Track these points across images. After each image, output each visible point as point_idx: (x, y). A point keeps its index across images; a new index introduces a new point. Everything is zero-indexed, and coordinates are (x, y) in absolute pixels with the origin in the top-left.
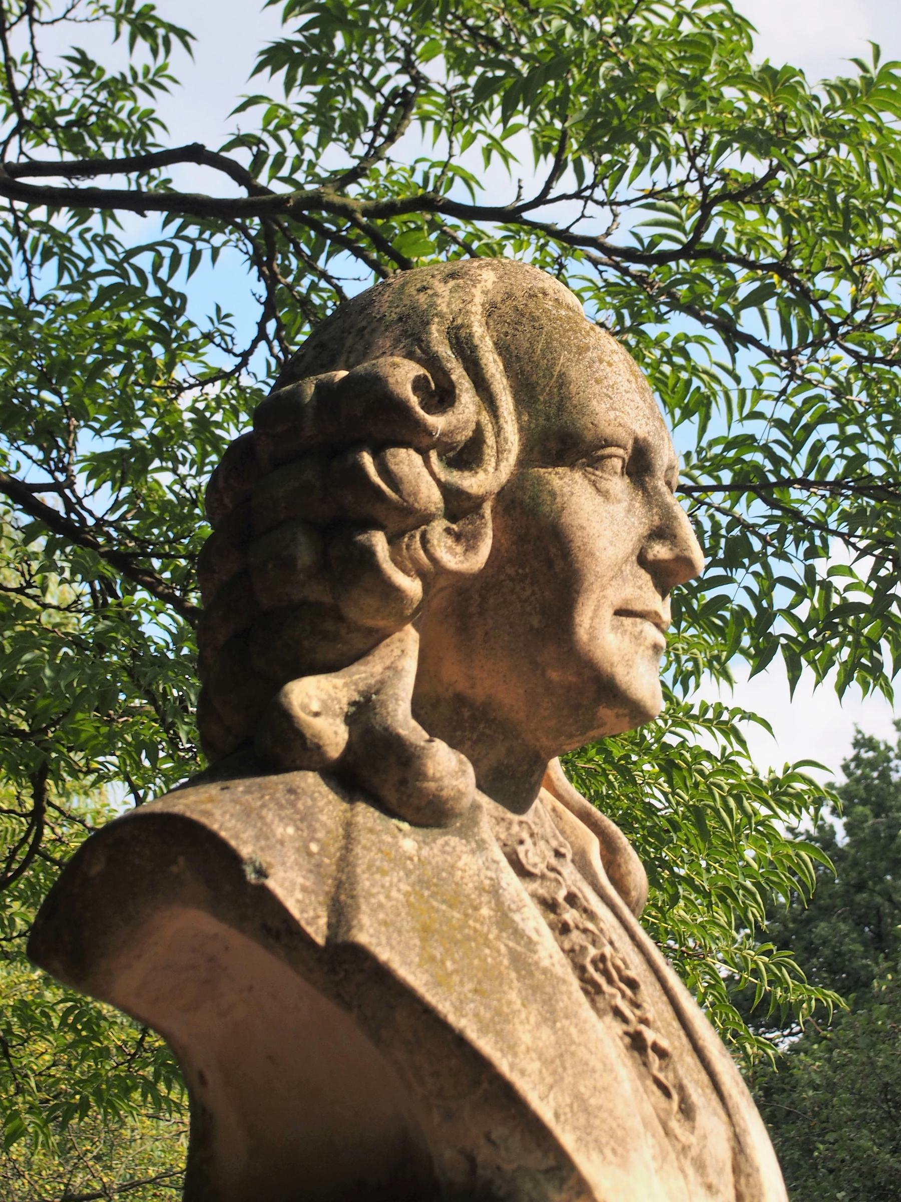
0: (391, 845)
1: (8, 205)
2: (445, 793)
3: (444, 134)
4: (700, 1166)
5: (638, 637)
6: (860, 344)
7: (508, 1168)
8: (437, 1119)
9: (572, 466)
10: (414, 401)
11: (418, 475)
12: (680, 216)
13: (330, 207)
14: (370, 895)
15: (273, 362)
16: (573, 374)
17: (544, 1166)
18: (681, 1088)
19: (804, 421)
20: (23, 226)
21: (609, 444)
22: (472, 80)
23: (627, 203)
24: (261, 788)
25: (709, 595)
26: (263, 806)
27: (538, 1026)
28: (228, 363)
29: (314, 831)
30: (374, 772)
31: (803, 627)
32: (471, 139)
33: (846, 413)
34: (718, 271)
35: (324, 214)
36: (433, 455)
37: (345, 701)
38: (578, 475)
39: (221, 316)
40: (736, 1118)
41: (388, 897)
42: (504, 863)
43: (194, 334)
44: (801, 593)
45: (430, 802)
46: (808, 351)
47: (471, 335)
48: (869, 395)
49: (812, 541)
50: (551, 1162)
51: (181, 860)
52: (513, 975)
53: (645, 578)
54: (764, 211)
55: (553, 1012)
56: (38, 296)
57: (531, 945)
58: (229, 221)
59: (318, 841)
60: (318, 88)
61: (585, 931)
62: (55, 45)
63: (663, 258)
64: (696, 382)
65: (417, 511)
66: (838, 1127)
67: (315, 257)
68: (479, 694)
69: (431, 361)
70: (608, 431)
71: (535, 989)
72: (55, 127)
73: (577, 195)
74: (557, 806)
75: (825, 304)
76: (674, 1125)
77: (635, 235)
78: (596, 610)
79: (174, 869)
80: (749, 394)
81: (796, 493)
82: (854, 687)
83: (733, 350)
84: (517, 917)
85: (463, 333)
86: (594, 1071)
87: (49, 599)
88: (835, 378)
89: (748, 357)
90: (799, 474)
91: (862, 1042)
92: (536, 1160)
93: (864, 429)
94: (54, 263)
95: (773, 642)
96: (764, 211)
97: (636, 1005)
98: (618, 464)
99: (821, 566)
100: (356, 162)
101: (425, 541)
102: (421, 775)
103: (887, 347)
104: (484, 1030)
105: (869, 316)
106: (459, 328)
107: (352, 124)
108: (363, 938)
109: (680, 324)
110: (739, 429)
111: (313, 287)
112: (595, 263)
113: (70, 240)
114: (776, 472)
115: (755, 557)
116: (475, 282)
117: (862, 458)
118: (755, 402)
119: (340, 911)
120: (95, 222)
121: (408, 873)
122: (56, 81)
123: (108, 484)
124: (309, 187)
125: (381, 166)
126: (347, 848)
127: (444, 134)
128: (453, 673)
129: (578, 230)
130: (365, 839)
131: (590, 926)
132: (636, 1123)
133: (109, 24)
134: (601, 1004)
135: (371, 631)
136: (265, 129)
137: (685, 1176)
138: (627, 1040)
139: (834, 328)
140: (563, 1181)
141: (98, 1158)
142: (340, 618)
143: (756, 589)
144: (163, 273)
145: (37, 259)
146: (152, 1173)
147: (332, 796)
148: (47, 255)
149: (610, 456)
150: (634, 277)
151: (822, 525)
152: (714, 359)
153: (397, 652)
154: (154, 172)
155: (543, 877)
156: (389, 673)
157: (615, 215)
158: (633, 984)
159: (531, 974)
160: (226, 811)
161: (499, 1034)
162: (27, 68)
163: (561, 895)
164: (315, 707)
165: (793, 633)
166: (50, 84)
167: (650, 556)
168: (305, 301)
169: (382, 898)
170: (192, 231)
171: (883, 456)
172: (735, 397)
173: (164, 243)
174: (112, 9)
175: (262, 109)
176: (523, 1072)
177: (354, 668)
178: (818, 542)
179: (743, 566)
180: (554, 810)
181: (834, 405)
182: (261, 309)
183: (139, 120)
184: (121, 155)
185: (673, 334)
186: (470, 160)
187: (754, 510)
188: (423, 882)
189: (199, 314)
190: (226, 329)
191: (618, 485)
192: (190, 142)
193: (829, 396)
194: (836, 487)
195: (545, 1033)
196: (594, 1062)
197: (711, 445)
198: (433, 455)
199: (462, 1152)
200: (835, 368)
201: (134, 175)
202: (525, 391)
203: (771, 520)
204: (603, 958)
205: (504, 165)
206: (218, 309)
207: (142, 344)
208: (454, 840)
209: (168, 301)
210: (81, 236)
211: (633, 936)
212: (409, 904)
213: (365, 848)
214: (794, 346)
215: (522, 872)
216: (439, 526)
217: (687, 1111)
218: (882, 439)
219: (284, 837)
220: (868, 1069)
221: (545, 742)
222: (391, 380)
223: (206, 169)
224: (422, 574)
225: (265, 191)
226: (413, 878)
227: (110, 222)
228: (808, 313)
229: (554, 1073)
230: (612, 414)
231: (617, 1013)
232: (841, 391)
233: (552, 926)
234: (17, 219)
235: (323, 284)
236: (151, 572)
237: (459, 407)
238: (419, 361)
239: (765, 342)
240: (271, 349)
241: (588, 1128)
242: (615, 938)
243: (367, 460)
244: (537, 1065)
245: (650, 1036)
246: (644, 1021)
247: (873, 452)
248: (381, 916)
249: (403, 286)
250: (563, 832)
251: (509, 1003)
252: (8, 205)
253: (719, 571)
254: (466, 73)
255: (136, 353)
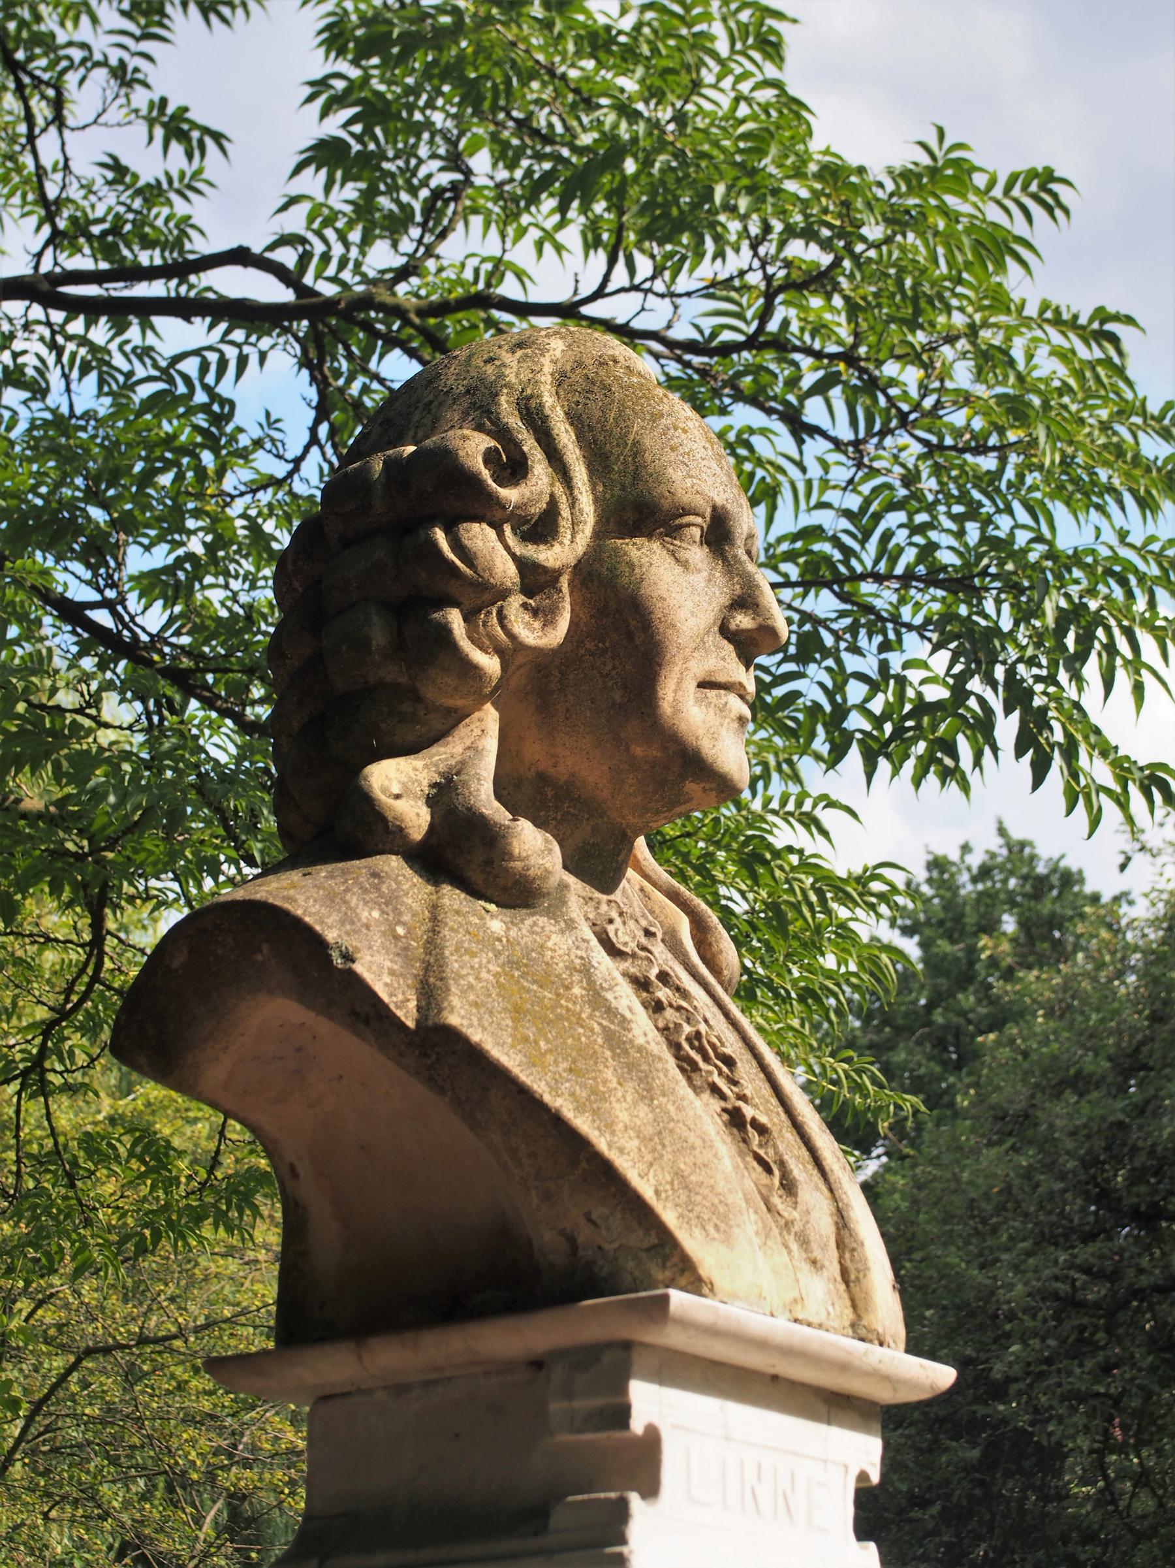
0: (479, 929)
1: (43, 318)
2: (531, 872)
3: (493, 228)
4: (804, 1242)
5: (723, 709)
6: (929, 431)
7: (610, 1247)
8: (535, 1201)
9: (650, 536)
10: (486, 474)
11: (492, 549)
12: (739, 305)
13: (380, 307)
14: (459, 976)
15: (326, 467)
16: (647, 442)
17: (646, 1245)
18: (782, 1164)
19: (872, 509)
20: (60, 340)
21: (687, 512)
22: (518, 174)
23: (688, 294)
24: (344, 872)
25: (779, 691)
26: (347, 890)
27: (635, 1103)
28: (280, 470)
29: (400, 914)
30: (458, 852)
31: (878, 722)
32: (522, 232)
33: (914, 501)
34: (780, 360)
35: (373, 314)
36: (507, 529)
37: (425, 783)
38: (656, 545)
39: (270, 421)
40: (838, 1193)
41: (478, 978)
42: (594, 942)
43: (244, 441)
44: (875, 687)
45: (517, 882)
46: (875, 440)
47: (541, 405)
48: (940, 483)
49: (885, 635)
50: (654, 1240)
51: (265, 948)
52: (608, 1054)
53: (729, 648)
54: (828, 297)
55: (649, 1090)
56: (79, 411)
57: (624, 1022)
58: (276, 324)
59: (404, 924)
60: (363, 185)
61: (679, 1009)
62: (86, 153)
63: (727, 350)
64: (760, 473)
65: (494, 586)
66: (924, 1246)
67: (366, 358)
68: (562, 772)
69: (502, 433)
70: (686, 499)
71: (631, 1067)
72: (90, 237)
73: (635, 288)
74: (644, 889)
75: (893, 392)
76: (776, 1200)
77: (697, 327)
78: (679, 683)
79: (259, 957)
80: (816, 484)
81: (867, 587)
82: (932, 779)
83: (800, 442)
84: (609, 996)
85: (533, 403)
86: (693, 1148)
87: (106, 716)
88: (903, 466)
89: (815, 447)
90: (869, 564)
91: (946, 1159)
92: (638, 1239)
93: (934, 517)
94: (93, 377)
95: (848, 737)
96: (828, 297)
97: (734, 1082)
98: (696, 532)
99: (896, 661)
100: (404, 260)
101: (501, 617)
102: (508, 855)
103: (958, 433)
104: (580, 1108)
105: (938, 402)
106: (529, 398)
107: (395, 226)
108: (454, 1020)
109: (744, 415)
110: (807, 520)
111: (365, 389)
112: (657, 356)
113: (109, 353)
114: (846, 562)
115: (826, 653)
116: (543, 351)
117: (933, 547)
118: (822, 492)
119: (430, 993)
120: (134, 333)
121: (497, 954)
122: (89, 189)
123: (159, 603)
124: (360, 289)
125: (431, 264)
126: (434, 931)
127: (493, 228)
128: (535, 752)
129: (638, 324)
130: (451, 921)
131: (684, 1004)
132: (738, 1199)
133: (142, 128)
134: (698, 1082)
135: (449, 711)
136: (308, 228)
137: (790, 1252)
138: (726, 1117)
139: (903, 417)
140: (666, 1258)
141: (172, 1299)
142: (418, 699)
143: (829, 684)
144: (210, 379)
145: (75, 374)
146: (227, 1313)
147: (416, 879)
148: (85, 369)
149: (689, 525)
150: (697, 370)
151: (896, 619)
152: (780, 449)
153: (477, 732)
154: (193, 278)
155: (634, 956)
156: (470, 753)
157: (676, 307)
158: (729, 1061)
159: (626, 1052)
160: (309, 896)
161: (595, 1112)
162: (58, 176)
163: (653, 973)
164: (396, 790)
165: (867, 727)
166: (82, 192)
167: (733, 626)
168: (357, 404)
169: (471, 979)
170: (238, 335)
171: (956, 544)
172: (801, 487)
173: (210, 348)
174: (144, 111)
175: (304, 208)
176: (621, 1150)
177: (433, 749)
178: (891, 636)
179: (815, 661)
180: (642, 890)
181: (903, 492)
182: (312, 414)
183: (177, 226)
184: (158, 261)
185: (737, 426)
186: (522, 253)
187: (824, 603)
188: (512, 963)
189: (248, 420)
190: (276, 435)
191: (698, 554)
192: (235, 245)
193: (897, 483)
194: (908, 578)
195: (643, 1110)
196: (693, 1138)
197: (780, 540)
198: (507, 529)
199: (562, 1232)
200: (903, 455)
201: (174, 283)
202: (598, 461)
203: (842, 614)
204: (698, 1035)
205: (554, 263)
206: (268, 415)
207: (190, 451)
208: (542, 921)
209: (216, 408)
210: (121, 348)
211: (727, 1014)
212: (500, 985)
213: (452, 929)
214: (861, 435)
215: (614, 951)
216: (515, 602)
217: (789, 1186)
218: (953, 527)
219: (367, 918)
220: (953, 1185)
221: (631, 819)
222: (461, 453)
223: (252, 272)
224: (500, 651)
225: (310, 292)
226: (502, 959)
227: (149, 333)
228: (875, 400)
229: (654, 1150)
230: (689, 482)
231: (715, 1090)
232: (910, 479)
233: (645, 1005)
234: (53, 333)
235: (375, 386)
236: (206, 686)
237: (532, 479)
238: (488, 433)
239: (832, 433)
240: (323, 454)
241: (690, 1205)
242: (709, 1016)
243: (440, 536)
244: (636, 1142)
245: (749, 1112)
246: (742, 1097)
247: (945, 540)
248: (472, 997)
249: (470, 357)
250: (652, 912)
251: (605, 1082)
252: (43, 318)
253: (791, 667)
254: (512, 166)
255: (185, 461)
